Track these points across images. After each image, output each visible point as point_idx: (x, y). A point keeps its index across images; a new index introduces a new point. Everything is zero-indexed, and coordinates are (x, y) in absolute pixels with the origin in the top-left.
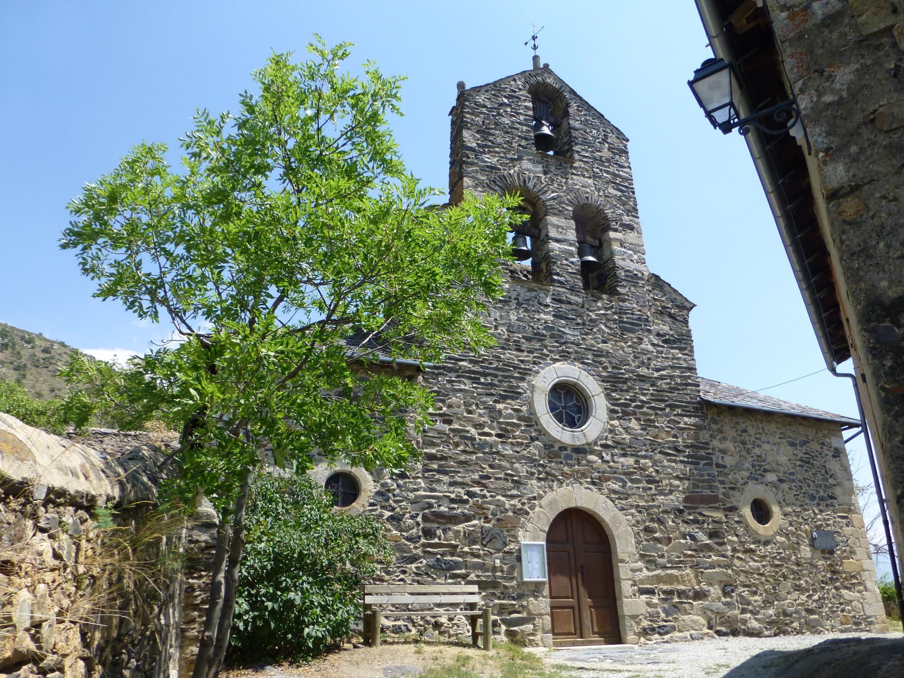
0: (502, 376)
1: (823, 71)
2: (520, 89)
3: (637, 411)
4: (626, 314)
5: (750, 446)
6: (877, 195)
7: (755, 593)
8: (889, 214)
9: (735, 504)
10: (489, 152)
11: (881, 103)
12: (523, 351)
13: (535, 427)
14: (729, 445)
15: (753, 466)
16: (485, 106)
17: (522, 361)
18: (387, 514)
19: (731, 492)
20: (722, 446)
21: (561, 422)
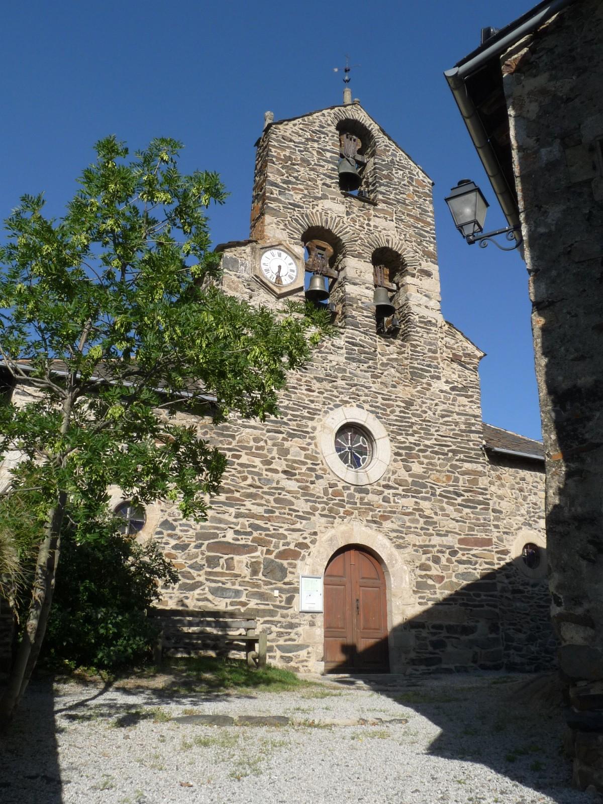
0: (292, 415)
1: (541, 207)
2: (329, 125)
3: (421, 454)
4: (417, 360)
5: (527, 494)
6: (565, 311)
7: (520, 631)
8: (571, 327)
9: (508, 547)
10: (294, 189)
11: (577, 240)
12: (313, 391)
13: (321, 466)
14: (506, 491)
15: (528, 512)
16: (291, 141)
17: (312, 401)
18: (173, 542)
19: (505, 536)
20: (500, 492)
21: (346, 462)
